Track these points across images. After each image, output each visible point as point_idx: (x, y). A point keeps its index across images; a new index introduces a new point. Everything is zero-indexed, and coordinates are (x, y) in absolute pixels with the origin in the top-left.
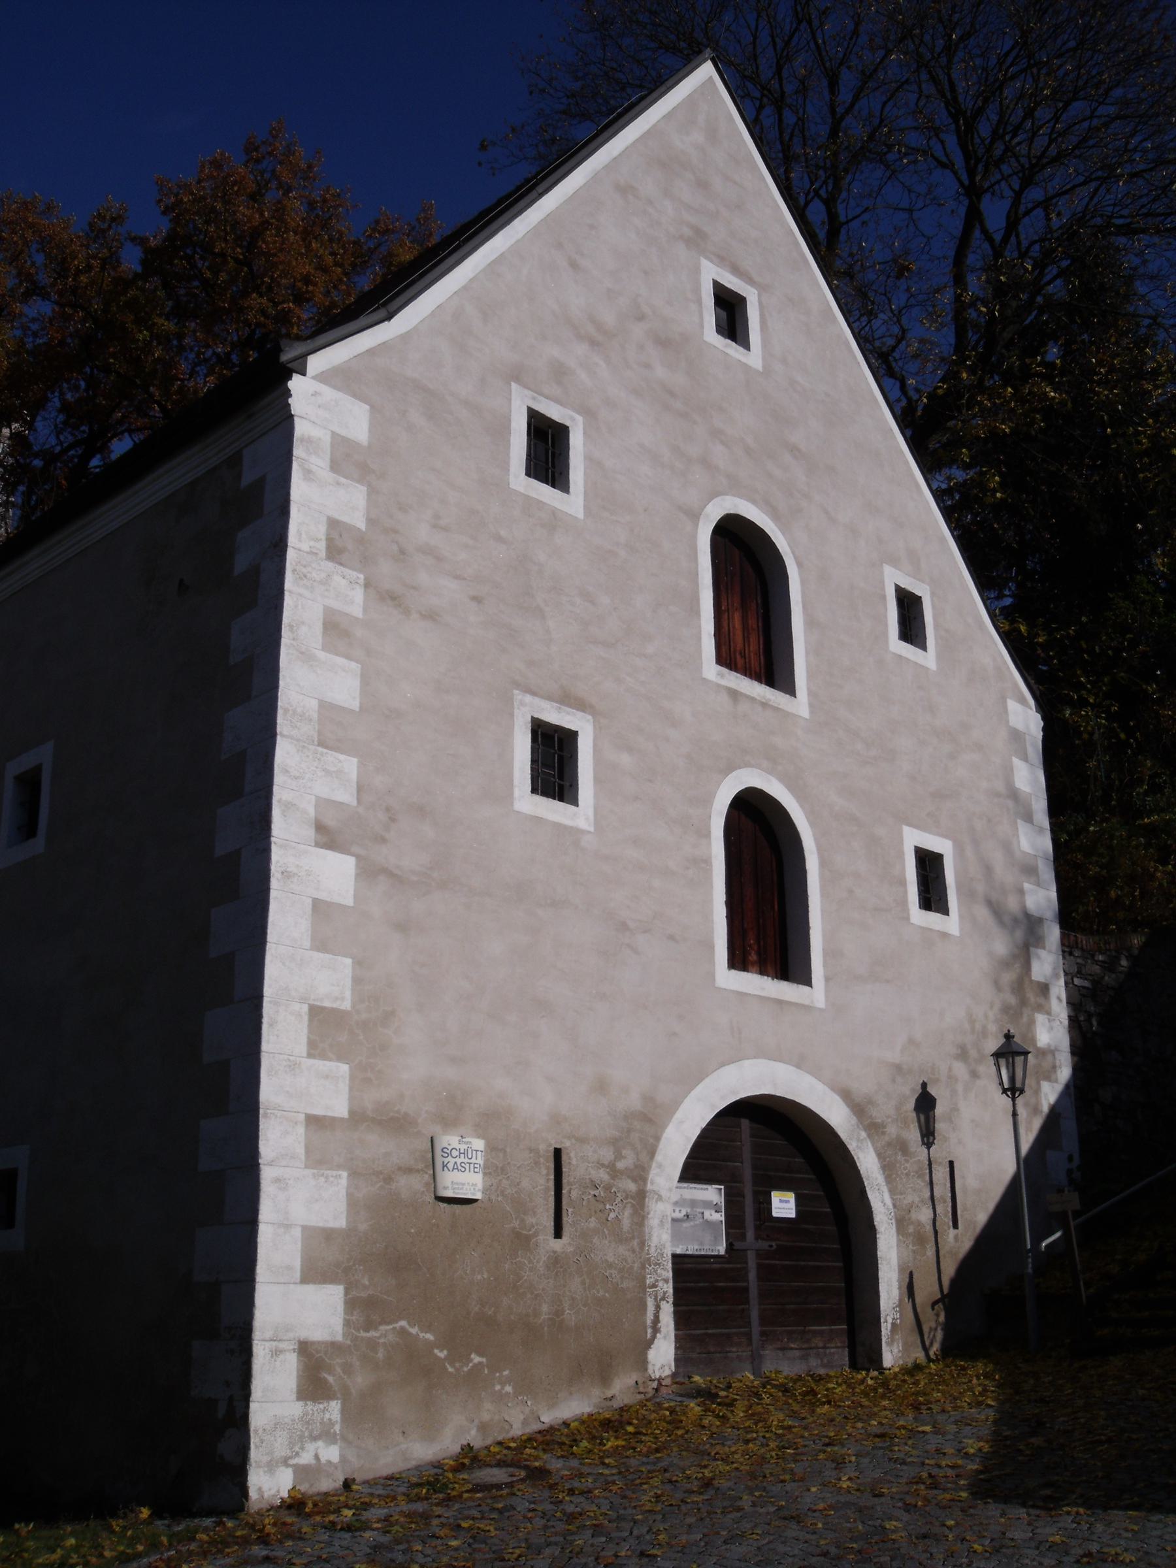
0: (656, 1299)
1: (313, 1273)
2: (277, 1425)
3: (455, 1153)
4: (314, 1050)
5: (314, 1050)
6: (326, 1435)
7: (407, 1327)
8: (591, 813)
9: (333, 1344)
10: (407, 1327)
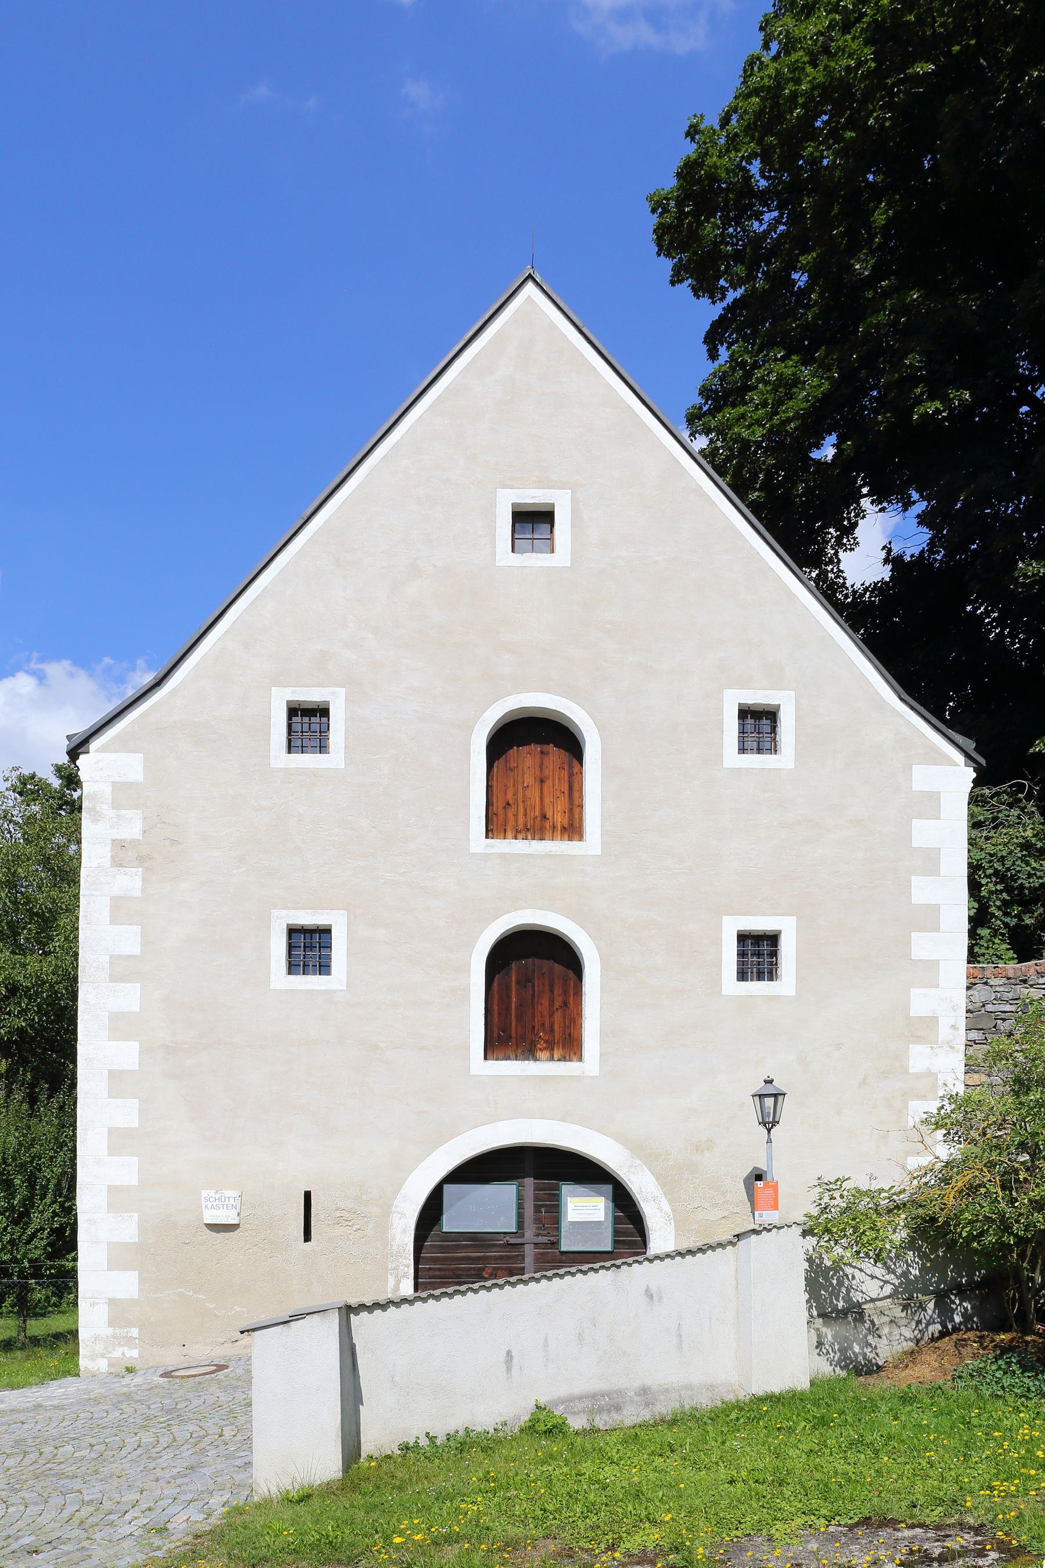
0: (397, 1276)
1: (114, 1264)
2: (96, 1338)
3: (211, 1199)
4: (112, 1151)
5: (112, 1151)
6: (129, 1341)
7: (185, 1292)
8: (344, 978)
9: (132, 1300)
10: (185, 1292)
